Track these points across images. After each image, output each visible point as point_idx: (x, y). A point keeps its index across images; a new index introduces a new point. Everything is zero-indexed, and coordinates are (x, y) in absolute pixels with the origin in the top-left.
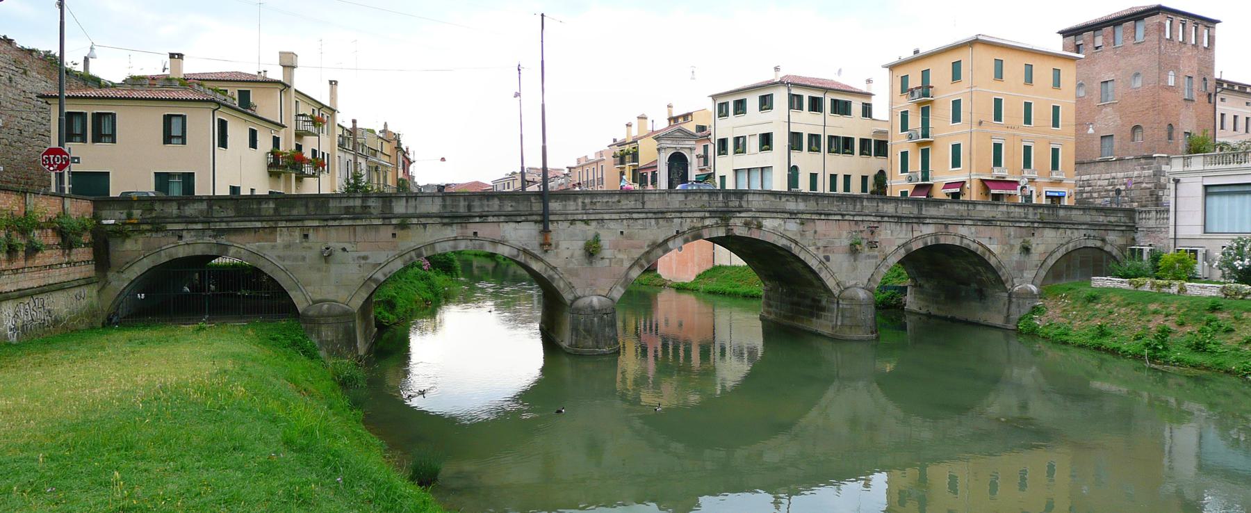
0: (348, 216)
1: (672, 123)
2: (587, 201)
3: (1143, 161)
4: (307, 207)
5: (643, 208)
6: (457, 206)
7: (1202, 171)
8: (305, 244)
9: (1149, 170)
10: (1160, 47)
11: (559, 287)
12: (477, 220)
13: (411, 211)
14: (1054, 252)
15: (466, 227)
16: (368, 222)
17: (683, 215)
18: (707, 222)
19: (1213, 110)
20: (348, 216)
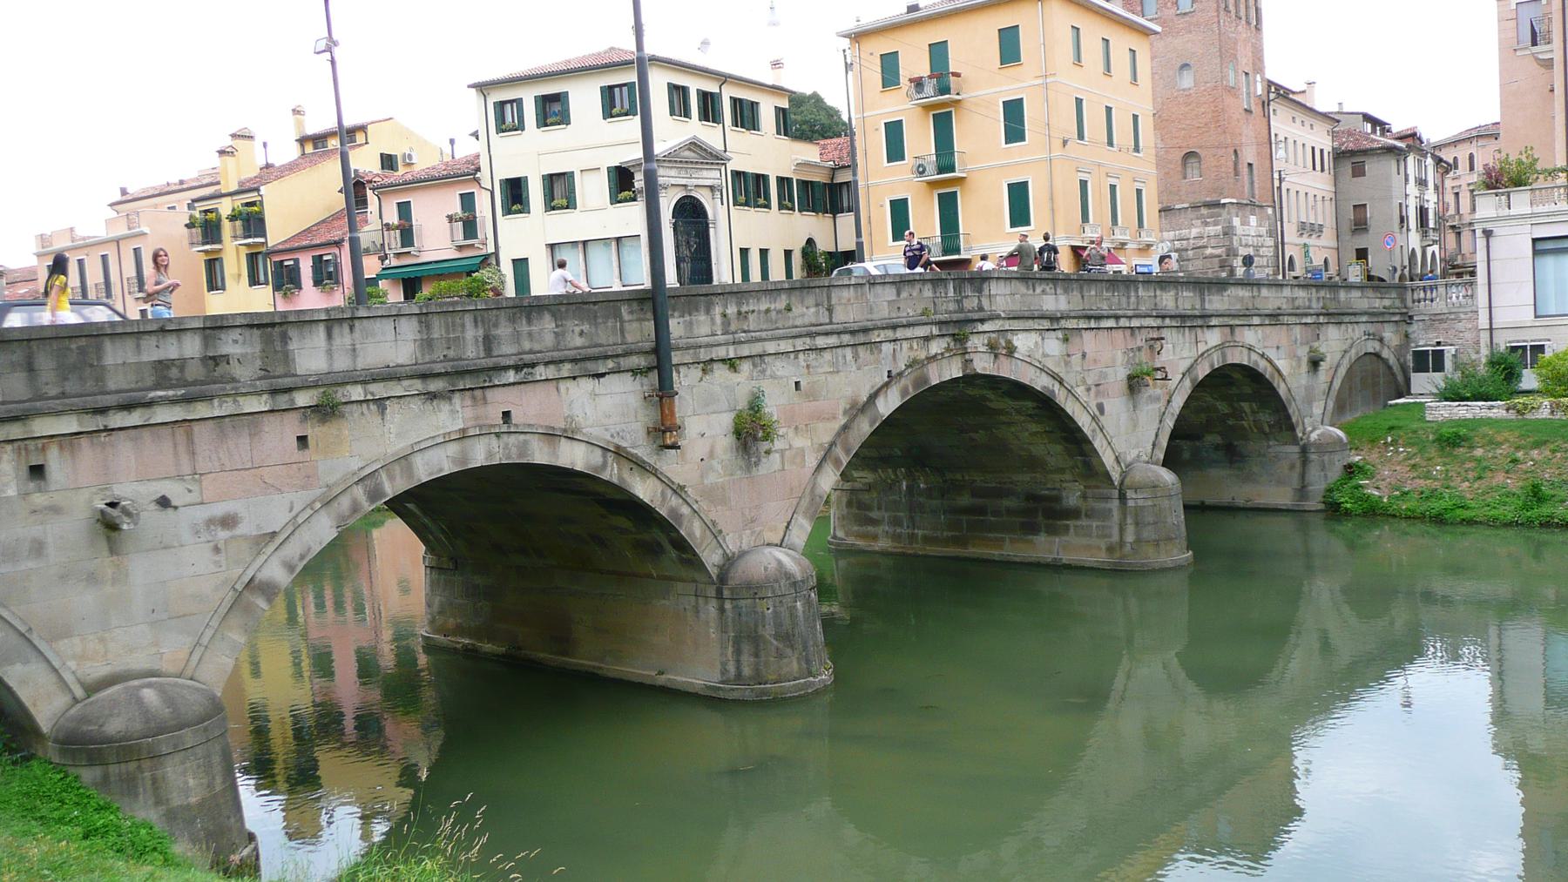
0: (171, 393)
1: (309, 149)
2: (732, 310)
3: (1204, 211)
4: (30, 368)
5: (831, 323)
6: (458, 341)
7: (1533, 215)
8: (39, 499)
9: (1215, 225)
10: (1219, 22)
11: (691, 534)
12: (511, 376)
13: (342, 363)
14: (1338, 366)
15: (484, 398)
16: (227, 408)
17: (900, 333)
18: (936, 347)
19: (1267, 127)
20: (171, 393)
